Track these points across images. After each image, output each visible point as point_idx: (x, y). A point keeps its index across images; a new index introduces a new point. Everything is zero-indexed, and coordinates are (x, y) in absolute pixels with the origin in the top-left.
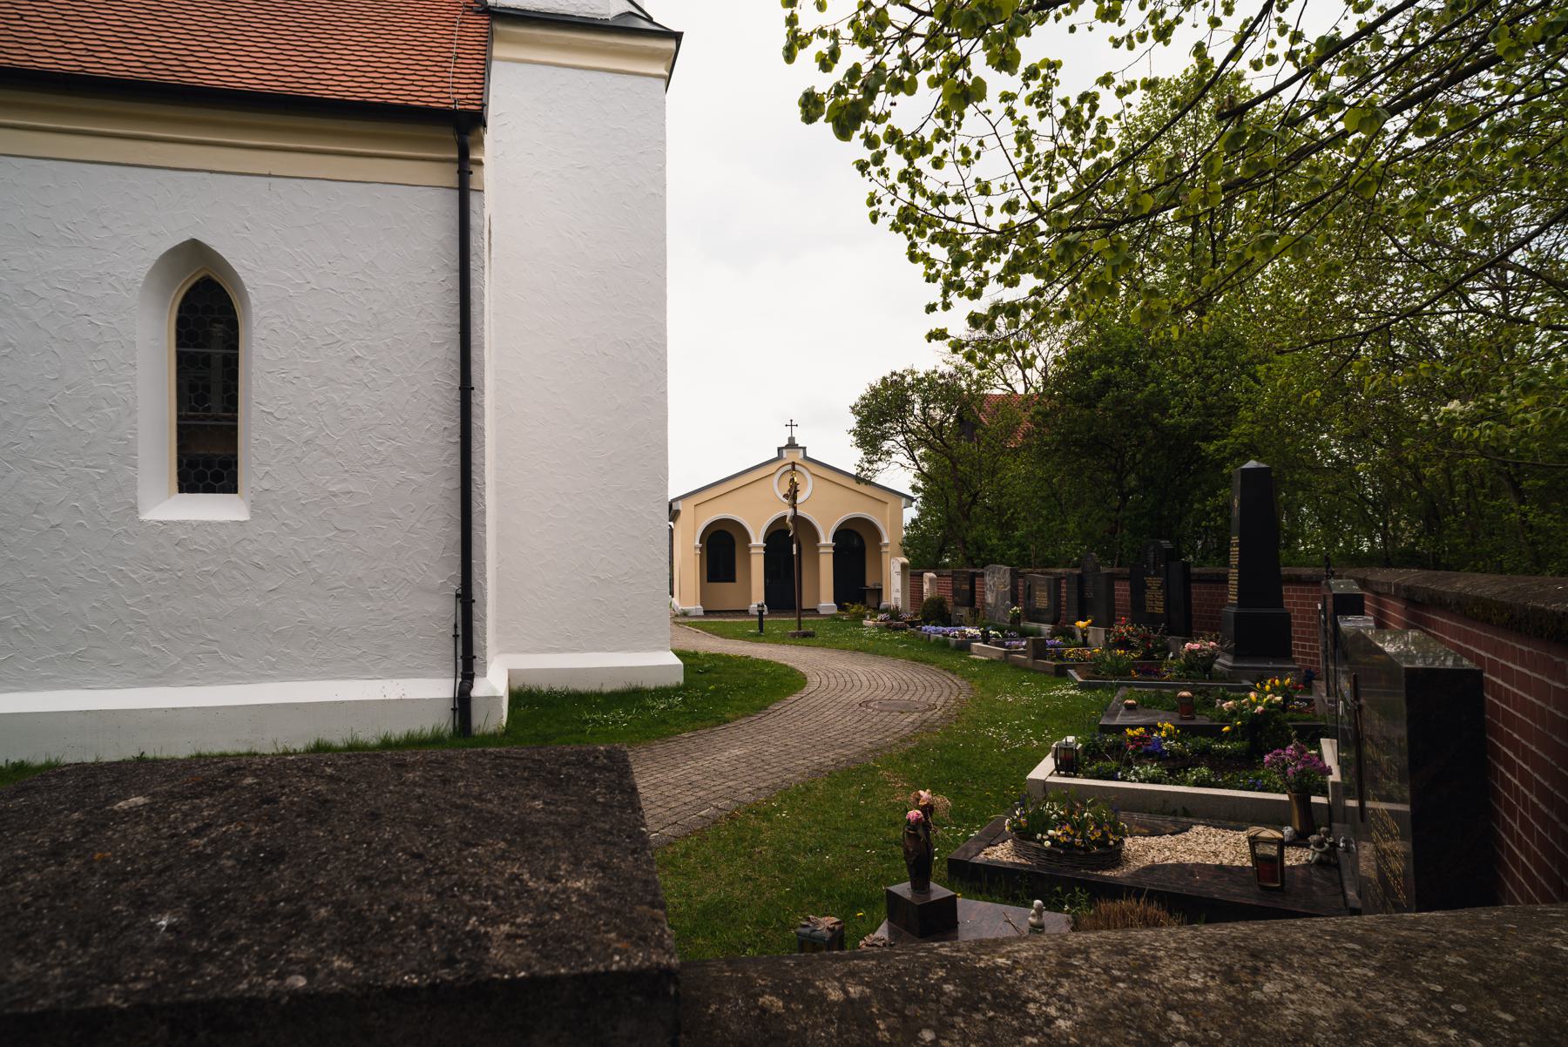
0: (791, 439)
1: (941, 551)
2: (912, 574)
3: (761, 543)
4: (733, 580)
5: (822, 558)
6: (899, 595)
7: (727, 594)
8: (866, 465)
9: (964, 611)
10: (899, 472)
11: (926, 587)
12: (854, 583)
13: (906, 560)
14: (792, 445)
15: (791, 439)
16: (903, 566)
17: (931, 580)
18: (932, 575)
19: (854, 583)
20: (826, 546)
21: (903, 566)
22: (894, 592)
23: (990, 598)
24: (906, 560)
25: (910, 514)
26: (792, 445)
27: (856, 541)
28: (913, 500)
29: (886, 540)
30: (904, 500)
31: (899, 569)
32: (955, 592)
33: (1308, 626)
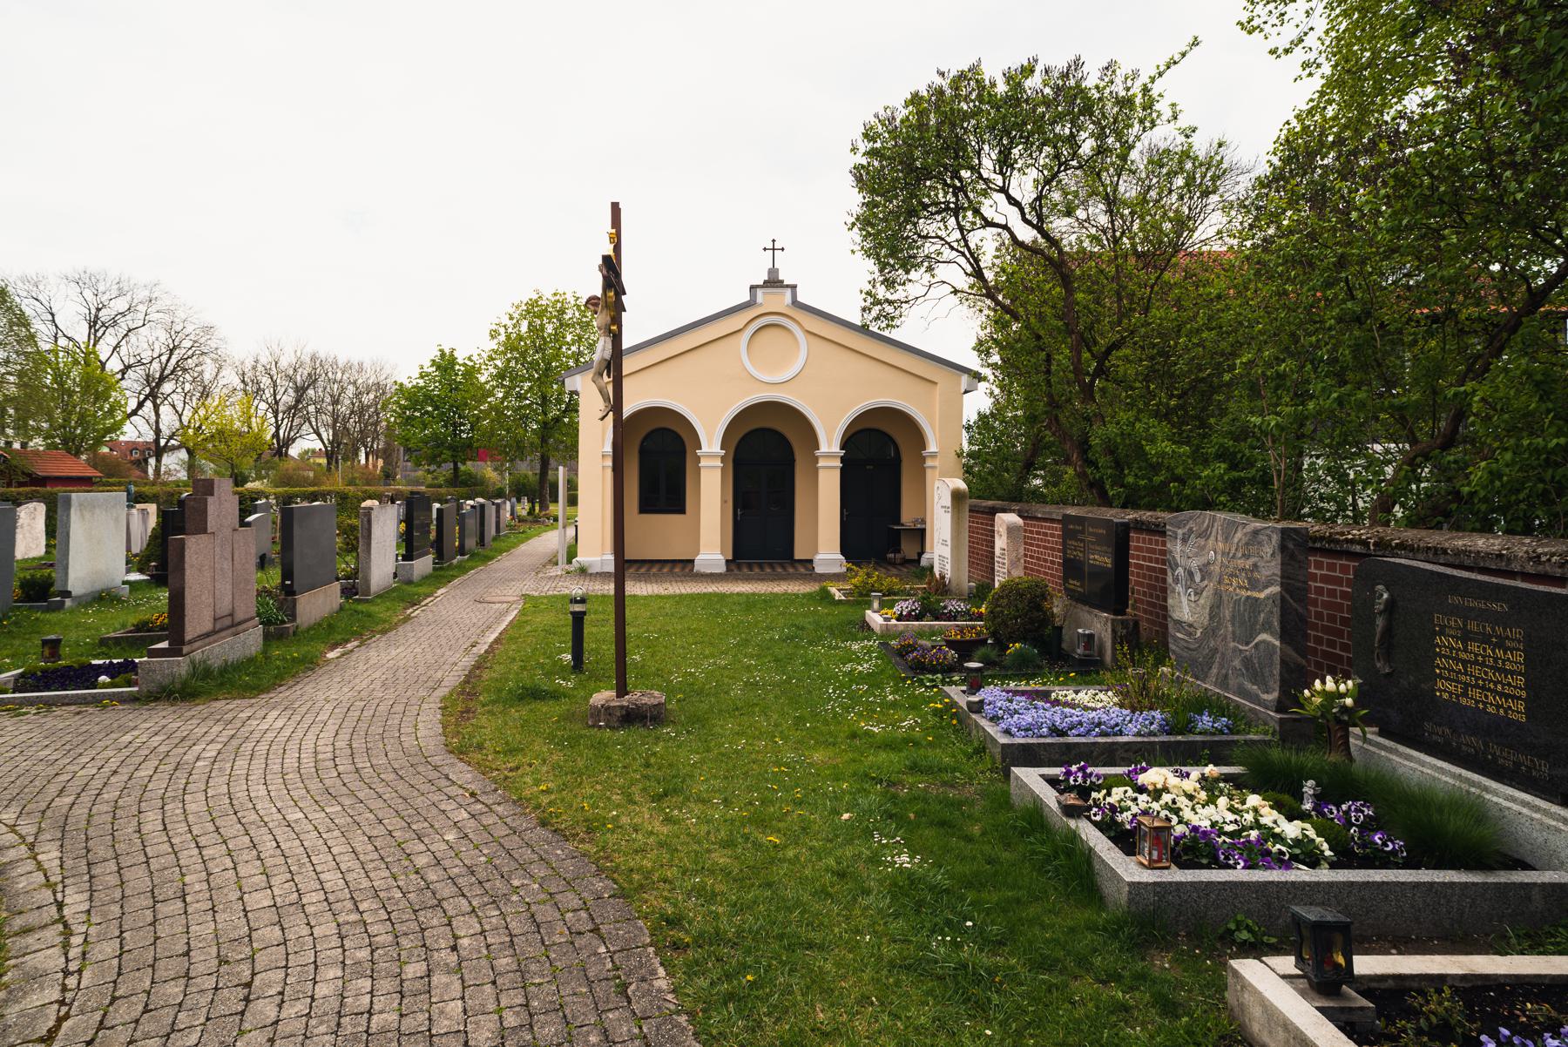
0: (773, 272)
1: (1029, 467)
2: (976, 507)
3: (716, 448)
4: (682, 511)
5: (822, 474)
6: (946, 552)
7: (656, 535)
8: (881, 292)
9: (1099, 625)
10: (946, 320)
11: (1000, 543)
12: (878, 529)
13: (963, 486)
14: (773, 282)
15: (773, 272)
16: (957, 496)
17: (1011, 530)
18: (1012, 518)
19: (878, 529)
20: (829, 456)
21: (957, 496)
22: (942, 549)
23: (1185, 607)
24: (963, 486)
25: (978, 402)
26: (773, 282)
27: (881, 450)
28: (978, 377)
29: (932, 447)
30: (965, 378)
31: (947, 501)
32: (1071, 568)
33: (1338, 581)
